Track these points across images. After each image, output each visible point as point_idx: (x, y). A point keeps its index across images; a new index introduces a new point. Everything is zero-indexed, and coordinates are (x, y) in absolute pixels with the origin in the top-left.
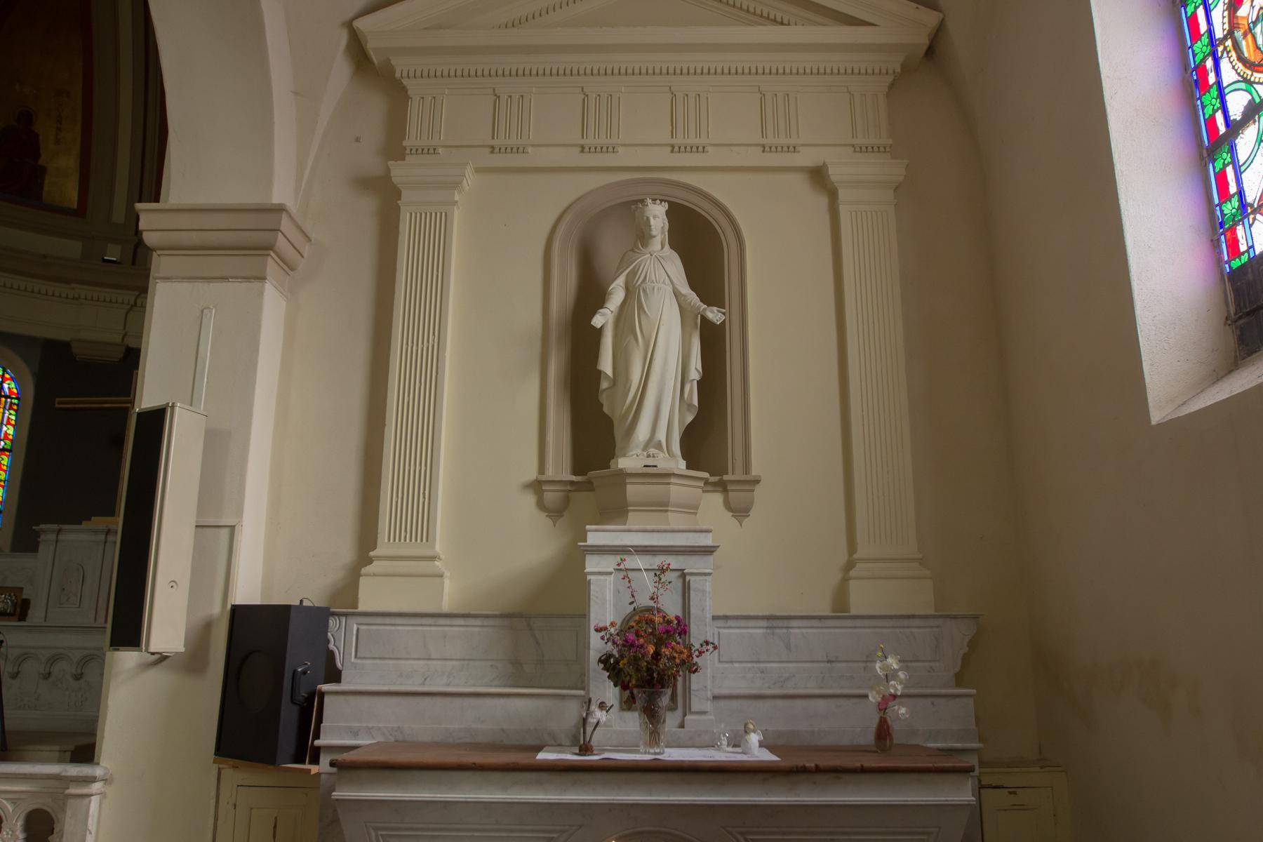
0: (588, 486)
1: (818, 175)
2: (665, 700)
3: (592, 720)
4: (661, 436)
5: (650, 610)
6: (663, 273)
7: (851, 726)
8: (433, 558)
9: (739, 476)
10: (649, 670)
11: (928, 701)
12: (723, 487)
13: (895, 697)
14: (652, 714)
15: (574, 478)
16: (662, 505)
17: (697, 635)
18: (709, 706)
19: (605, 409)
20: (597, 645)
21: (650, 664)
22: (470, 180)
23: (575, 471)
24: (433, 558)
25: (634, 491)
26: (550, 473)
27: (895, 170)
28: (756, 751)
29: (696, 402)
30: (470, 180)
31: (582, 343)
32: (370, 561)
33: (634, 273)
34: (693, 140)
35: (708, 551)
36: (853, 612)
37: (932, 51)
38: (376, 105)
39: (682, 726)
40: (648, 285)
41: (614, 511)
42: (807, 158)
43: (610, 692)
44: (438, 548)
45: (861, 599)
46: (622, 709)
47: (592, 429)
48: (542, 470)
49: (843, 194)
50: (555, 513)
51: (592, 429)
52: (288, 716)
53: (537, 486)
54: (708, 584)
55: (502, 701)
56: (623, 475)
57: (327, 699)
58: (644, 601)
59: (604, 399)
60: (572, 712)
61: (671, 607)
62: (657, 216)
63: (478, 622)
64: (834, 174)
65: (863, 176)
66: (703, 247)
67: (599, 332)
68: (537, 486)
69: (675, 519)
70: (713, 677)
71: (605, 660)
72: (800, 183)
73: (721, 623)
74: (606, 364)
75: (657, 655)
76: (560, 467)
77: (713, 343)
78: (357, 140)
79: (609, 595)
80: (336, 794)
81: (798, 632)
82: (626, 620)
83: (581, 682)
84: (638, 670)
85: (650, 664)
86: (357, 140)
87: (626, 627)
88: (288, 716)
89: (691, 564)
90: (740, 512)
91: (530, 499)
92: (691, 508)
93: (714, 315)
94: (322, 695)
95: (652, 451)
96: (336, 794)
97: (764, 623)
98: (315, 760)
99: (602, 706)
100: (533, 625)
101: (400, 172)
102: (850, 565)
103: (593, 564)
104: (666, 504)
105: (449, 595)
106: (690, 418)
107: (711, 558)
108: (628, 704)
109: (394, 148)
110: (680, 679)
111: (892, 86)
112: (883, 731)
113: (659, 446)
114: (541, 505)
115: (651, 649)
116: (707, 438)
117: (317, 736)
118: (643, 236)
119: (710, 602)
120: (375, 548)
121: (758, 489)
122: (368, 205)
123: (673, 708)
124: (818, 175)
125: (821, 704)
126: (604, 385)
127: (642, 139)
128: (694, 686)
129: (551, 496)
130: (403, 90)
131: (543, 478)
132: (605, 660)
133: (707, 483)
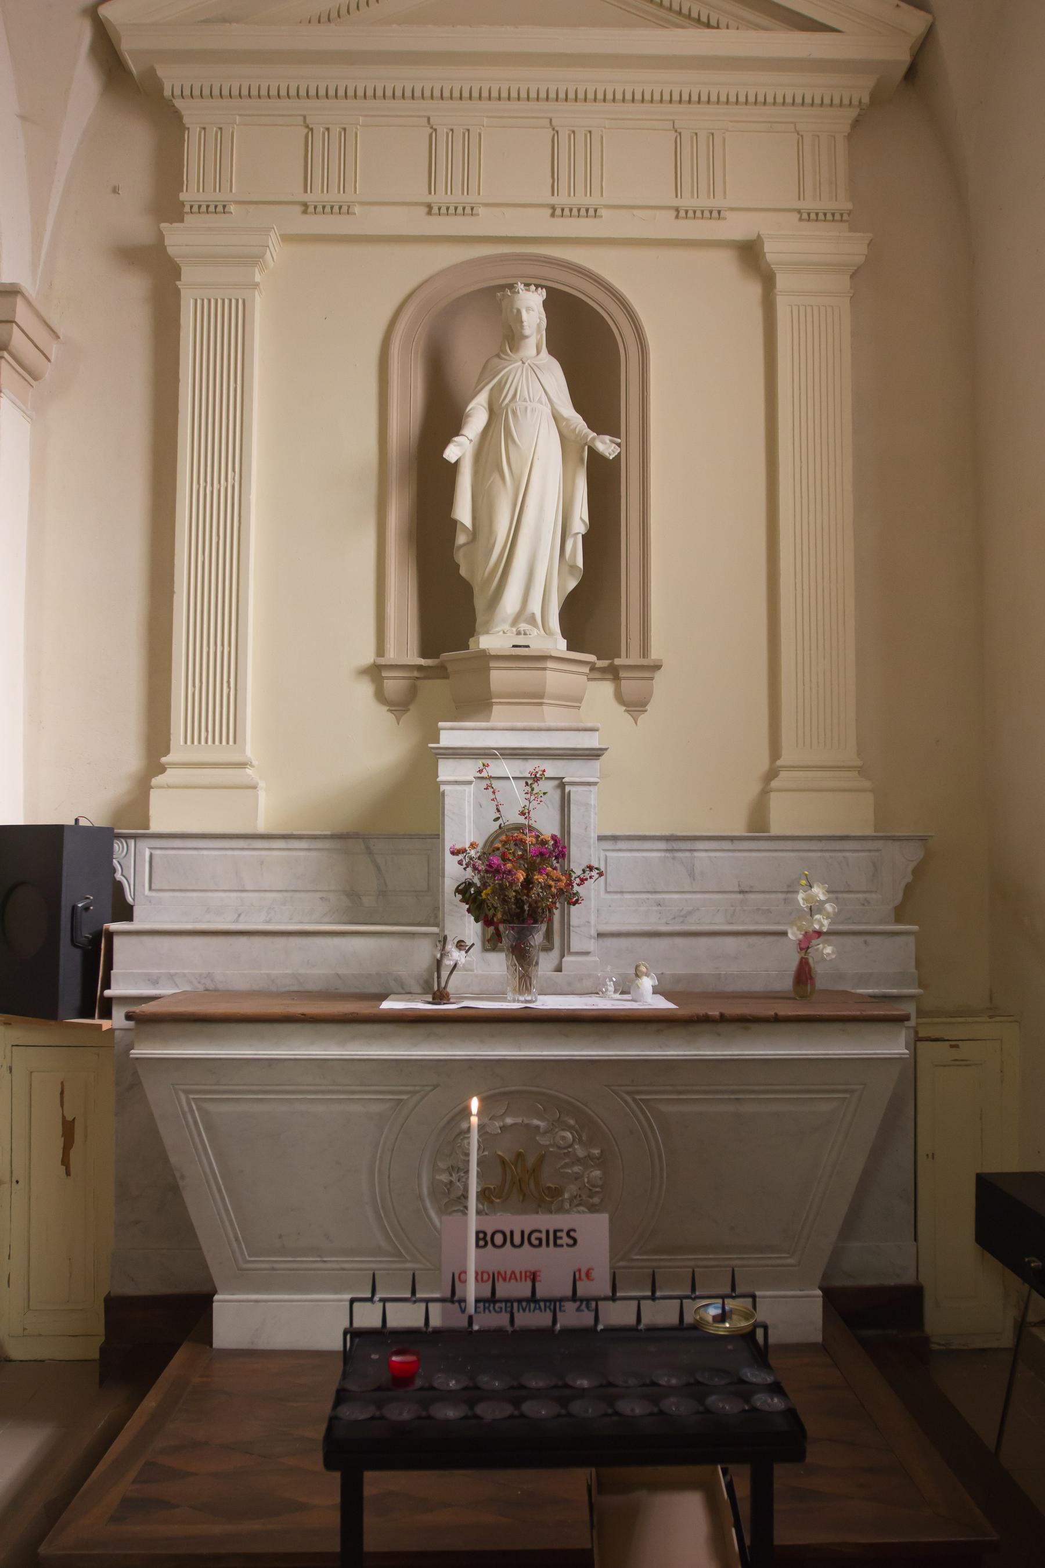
0: (441, 672)
1: (749, 253)
2: (538, 938)
3: (448, 962)
4: (535, 606)
5: (519, 828)
6: (539, 388)
7: (768, 968)
8: (242, 765)
9: (635, 660)
10: (519, 903)
11: (859, 940)
12: (613, 673)
13: (819, 933)
14: (521, 954)
15: (422, 662)
16: (535, 697)
17: (578, 858)
18: (591, 945)
19: (463, 572)
20: (454, 872)
21: (520, 893)
22: (275, 252)
23: (424, 654)
24: (242, 765)
25: (499, 678)
26: (392, 655)
27: (853, 248)
28: (647, 997)
29: (580, 562)
30: (275, 252)
31: (428, 482)
32: (162, 769)
33: (499, 388)
34: (581, 199)
35: (593, 754)
36: (774, 831)
37: (924, 48)
38: (135, 143)
39: (559, 969)
40: (519, 405)
41: (475, 704)
42: (736, 228)
43: (471, 929)
44: (250, 750)
45: (782, 817)
46: (485, 950)
47: (446, 599)
48: (380, 651)
49: (781, 281)
50: (399, 706)
51: (446, 599)
52: (69, 959)
53: (375, 672)
54: (593, 796)
55: (337, 941)
56: (485, 658)
57: (117, 941)
58: (512, 817)
59: (460, 557)
60: (423, 953)
61: (547, 824)
62: (531, 308)
63: (303, 844)
64: (772, 251)
65: (809, 252)
66: (592, 349)
67: (453, 468)
68: (375, 672)
69: (551, 715)
70: (595, 910)
71: (464, 891)
72: (726, 262)
73: (608, 845)
74: (463, 512)
75: (528, 883)
76: (404, 647)
77: (604, 481)
78: (115, 190)
79: (469, 810)
80: (135, 1053)
81: (703, 857)
82: (490, 841)
83: (435, 917)
84: (504, 901)
85: (520, 893)
86: (115, 190)
87: (490, 848)
88: (69, 959)
89: (572, 771)
90: (635, 706)
91: (365, 689)
92: (574, 701)
93: (606, 446)
94: (110, 936)
95: (523, 626)
96: (135, 1053)
97: (662, 845)
98: (107, 1014)
99: (460, 945)
100: (374, 848)
101: (178, 239)
102: (772, 774)
103: (447, 771)
104: (541, 696)
105: (265, 812)
106: (572, 584)
107: (597, 764)
108: (492, 943)
109: (167, 204)
110: (557, 912)
111: (856, 123)
112: (804, 975)
113: (532, 620)
114: (380, 696)
115: (521, 876)
116: (593, 612)
117: (107, 985)
118: (511, 336)
119: (595, 821)
120: (167, 751)
121: (658, 676)
122: (135, 286)
123: (548, 948)
124: (749, 253)
125: (730, 944)
126: (461, 539)
127: (512, 197)
128: (574, 921)
129: (394, 685)
130: (176, 116)
131: (382, 661)
132: (464, 891)
133: (593, 668)
